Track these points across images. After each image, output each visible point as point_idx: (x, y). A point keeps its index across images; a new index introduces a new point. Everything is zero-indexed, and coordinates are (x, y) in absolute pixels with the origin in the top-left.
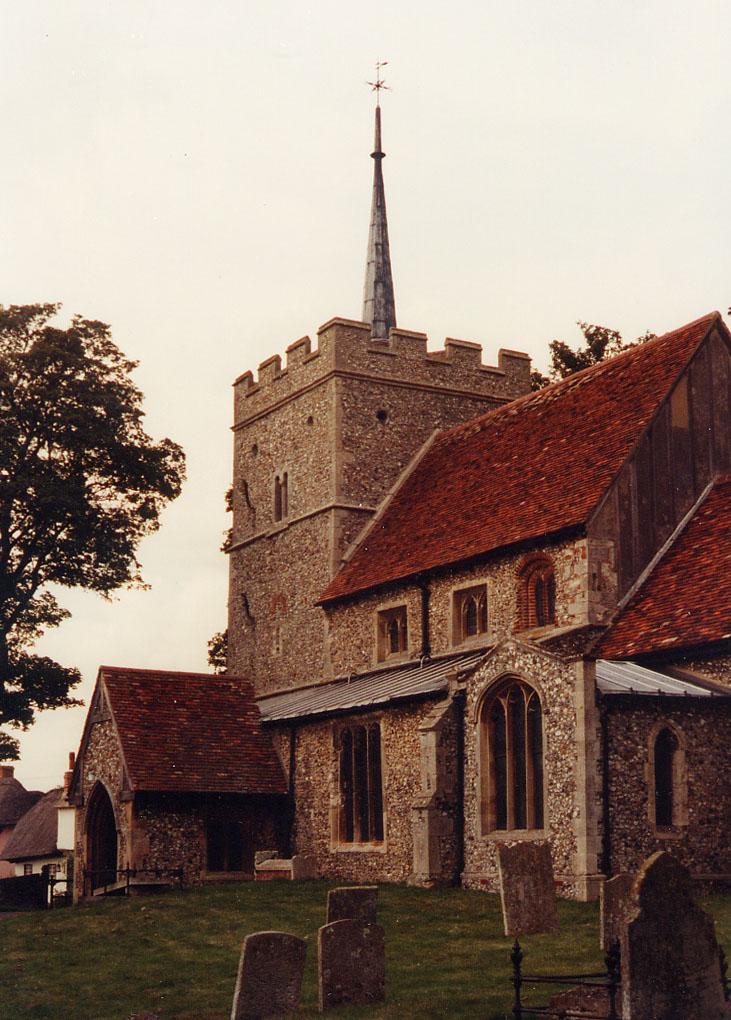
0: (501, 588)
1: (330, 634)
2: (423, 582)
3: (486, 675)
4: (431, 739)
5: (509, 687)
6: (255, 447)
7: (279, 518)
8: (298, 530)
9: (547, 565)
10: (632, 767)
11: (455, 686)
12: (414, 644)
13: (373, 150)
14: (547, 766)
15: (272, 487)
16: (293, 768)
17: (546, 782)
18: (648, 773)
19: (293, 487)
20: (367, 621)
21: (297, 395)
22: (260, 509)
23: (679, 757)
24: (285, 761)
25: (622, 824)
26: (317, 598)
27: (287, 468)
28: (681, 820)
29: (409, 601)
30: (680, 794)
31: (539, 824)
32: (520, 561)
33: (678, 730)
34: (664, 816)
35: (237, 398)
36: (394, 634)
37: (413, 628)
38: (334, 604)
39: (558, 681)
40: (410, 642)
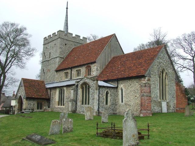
0: (83, 70)
1: (57, 75)
2: (71, 68)
3: (82, 82)
4: (72, 91)
5: (85, 84)
6: (46, 48)
7: (49, 58)
8: (52, 60)
9: (90, 67)
10: (103, 96)
11: (76, 84)
12: (69, 77)
13: (66, 7)
14: (90, 96)
15: (49, 54)
16: (50, 95)
17: (90, 98)
18: (105, 97)
19: (52, 54)
20: (62, 74)
21: (53, 41)
22: (47, 57)
23: (109, 95)
24: (49, 93)
25: (101, 104)
26: (55, 70)
27: (51, 51)
28: (109, 103)
29: (69, 71)
30: (123, 100)
31: (89, 104)
32: (86, 66)
33: (109, 91)
34: (107, 103)
35: (44, 40)
36: (66, 76)
37: (69, 75)
38: (57, 71)
39: (92, 83)
40: (69, 77)
